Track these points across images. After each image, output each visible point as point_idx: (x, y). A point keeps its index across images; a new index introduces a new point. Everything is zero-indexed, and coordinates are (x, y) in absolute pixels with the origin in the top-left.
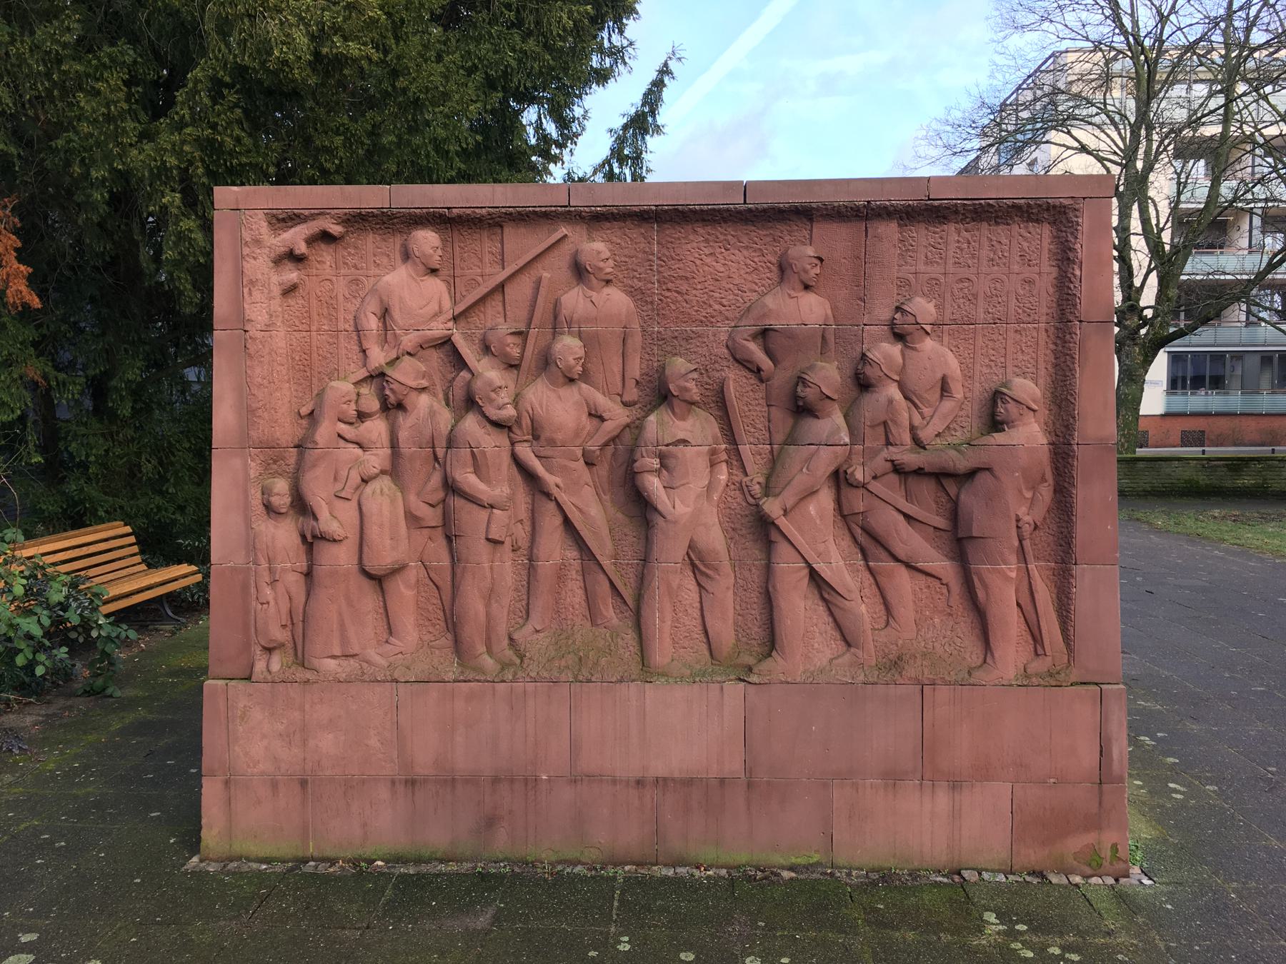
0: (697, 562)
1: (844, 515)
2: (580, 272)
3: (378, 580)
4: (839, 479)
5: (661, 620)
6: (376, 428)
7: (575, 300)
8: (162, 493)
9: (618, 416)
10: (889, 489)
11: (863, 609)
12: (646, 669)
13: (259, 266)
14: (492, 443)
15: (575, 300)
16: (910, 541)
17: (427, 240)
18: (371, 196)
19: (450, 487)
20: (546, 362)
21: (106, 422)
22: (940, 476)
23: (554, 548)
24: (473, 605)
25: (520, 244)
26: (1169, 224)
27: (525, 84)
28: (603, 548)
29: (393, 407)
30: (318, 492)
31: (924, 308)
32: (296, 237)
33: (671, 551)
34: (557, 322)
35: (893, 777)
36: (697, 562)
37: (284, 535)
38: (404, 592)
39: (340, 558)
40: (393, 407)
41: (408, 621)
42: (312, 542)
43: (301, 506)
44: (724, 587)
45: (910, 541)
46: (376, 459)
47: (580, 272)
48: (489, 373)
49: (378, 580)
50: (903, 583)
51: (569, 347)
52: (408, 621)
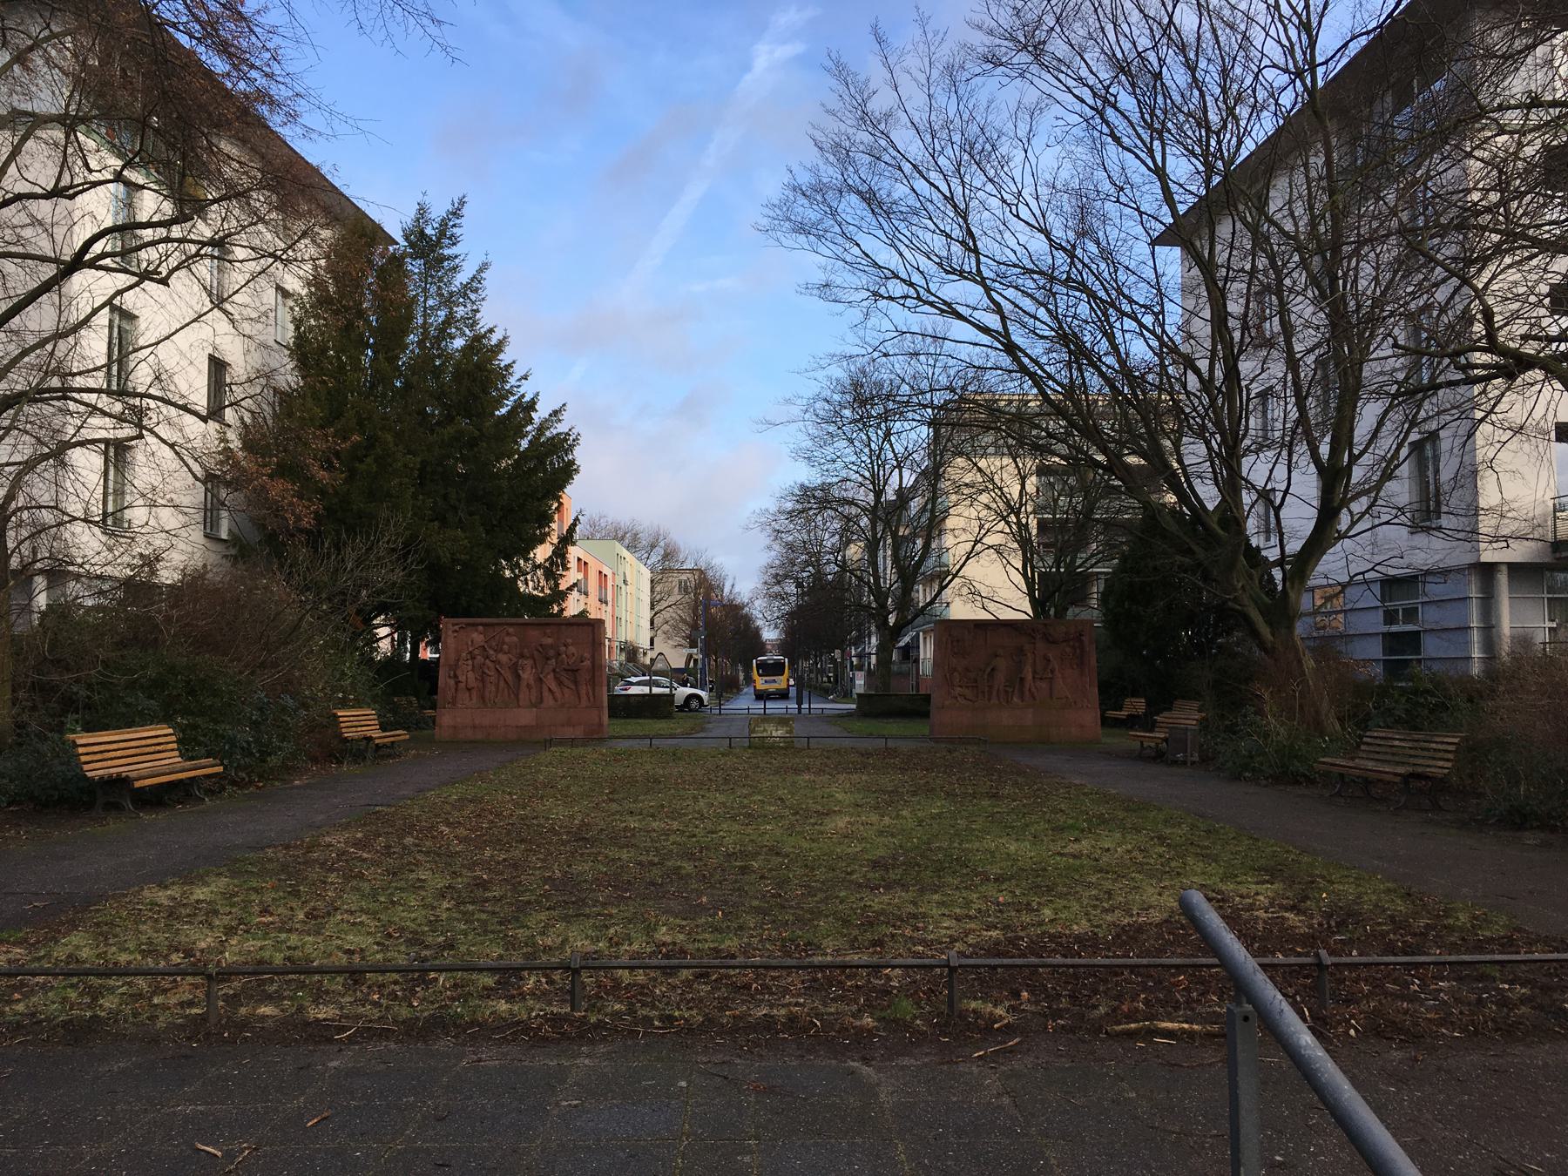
0: (528, 686)
1: (556, 678)
2: (508, 634)
3: (469, 690)
4: (554, 671)
5: (521, 696)
6: (470, 662)
7: (507, 639)
8: (1161, 72)
9: (514, 660)
10: (563, 673)
11: (558, 695)
12: (519, 706)
13: (450, 633)
14: (490, 664)
15: (507, 639)
16: (567, 682)
17: (481, 628)
18: (471, 620)
19: (483, 673)
20: (501, 650)
21: (377, 690)
22: (573, 671)
23: (502, 684)
24: (487, 694)
25: (498, 629)
26: (37, 591)
27: (604, 905)
28: (511, 684)
29: (473, 658)
30: (459, 673)
31: (570, 641)
32: (456, 627)
33: (524, 684)
34: (504, 643)
35: (563, 725)
36: (528, 686)
37: (452, 682)
38: (474, 693)
39: (462, 685)
40: (473, 658)
41: (474, 698)
42: (457, 683)
43: (456, 676)
44: (534, 691)
45: (567, 682)
46: (470, 668)
47: (508, 634)
48: (491, 652)
49: (469, 690)
50: (566, 690)
51: (505, 647)
52: (474, 698)
